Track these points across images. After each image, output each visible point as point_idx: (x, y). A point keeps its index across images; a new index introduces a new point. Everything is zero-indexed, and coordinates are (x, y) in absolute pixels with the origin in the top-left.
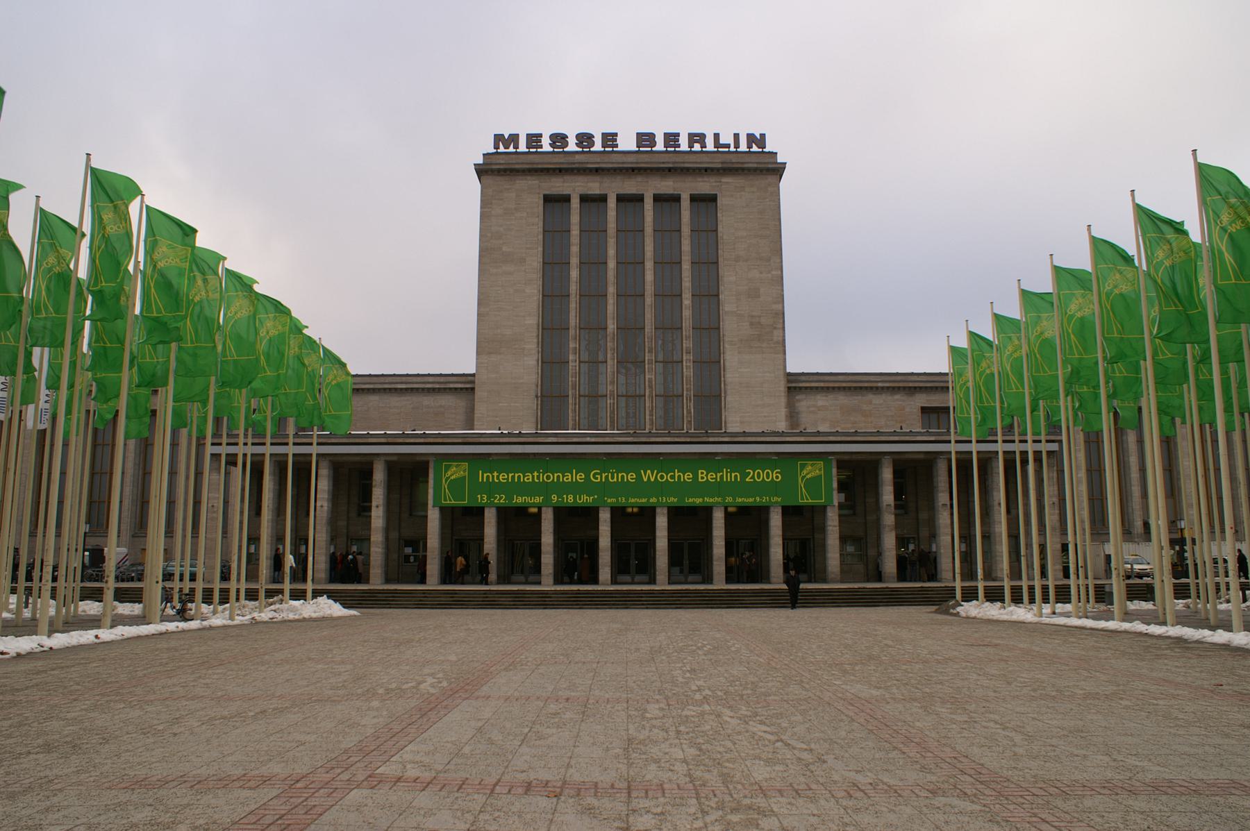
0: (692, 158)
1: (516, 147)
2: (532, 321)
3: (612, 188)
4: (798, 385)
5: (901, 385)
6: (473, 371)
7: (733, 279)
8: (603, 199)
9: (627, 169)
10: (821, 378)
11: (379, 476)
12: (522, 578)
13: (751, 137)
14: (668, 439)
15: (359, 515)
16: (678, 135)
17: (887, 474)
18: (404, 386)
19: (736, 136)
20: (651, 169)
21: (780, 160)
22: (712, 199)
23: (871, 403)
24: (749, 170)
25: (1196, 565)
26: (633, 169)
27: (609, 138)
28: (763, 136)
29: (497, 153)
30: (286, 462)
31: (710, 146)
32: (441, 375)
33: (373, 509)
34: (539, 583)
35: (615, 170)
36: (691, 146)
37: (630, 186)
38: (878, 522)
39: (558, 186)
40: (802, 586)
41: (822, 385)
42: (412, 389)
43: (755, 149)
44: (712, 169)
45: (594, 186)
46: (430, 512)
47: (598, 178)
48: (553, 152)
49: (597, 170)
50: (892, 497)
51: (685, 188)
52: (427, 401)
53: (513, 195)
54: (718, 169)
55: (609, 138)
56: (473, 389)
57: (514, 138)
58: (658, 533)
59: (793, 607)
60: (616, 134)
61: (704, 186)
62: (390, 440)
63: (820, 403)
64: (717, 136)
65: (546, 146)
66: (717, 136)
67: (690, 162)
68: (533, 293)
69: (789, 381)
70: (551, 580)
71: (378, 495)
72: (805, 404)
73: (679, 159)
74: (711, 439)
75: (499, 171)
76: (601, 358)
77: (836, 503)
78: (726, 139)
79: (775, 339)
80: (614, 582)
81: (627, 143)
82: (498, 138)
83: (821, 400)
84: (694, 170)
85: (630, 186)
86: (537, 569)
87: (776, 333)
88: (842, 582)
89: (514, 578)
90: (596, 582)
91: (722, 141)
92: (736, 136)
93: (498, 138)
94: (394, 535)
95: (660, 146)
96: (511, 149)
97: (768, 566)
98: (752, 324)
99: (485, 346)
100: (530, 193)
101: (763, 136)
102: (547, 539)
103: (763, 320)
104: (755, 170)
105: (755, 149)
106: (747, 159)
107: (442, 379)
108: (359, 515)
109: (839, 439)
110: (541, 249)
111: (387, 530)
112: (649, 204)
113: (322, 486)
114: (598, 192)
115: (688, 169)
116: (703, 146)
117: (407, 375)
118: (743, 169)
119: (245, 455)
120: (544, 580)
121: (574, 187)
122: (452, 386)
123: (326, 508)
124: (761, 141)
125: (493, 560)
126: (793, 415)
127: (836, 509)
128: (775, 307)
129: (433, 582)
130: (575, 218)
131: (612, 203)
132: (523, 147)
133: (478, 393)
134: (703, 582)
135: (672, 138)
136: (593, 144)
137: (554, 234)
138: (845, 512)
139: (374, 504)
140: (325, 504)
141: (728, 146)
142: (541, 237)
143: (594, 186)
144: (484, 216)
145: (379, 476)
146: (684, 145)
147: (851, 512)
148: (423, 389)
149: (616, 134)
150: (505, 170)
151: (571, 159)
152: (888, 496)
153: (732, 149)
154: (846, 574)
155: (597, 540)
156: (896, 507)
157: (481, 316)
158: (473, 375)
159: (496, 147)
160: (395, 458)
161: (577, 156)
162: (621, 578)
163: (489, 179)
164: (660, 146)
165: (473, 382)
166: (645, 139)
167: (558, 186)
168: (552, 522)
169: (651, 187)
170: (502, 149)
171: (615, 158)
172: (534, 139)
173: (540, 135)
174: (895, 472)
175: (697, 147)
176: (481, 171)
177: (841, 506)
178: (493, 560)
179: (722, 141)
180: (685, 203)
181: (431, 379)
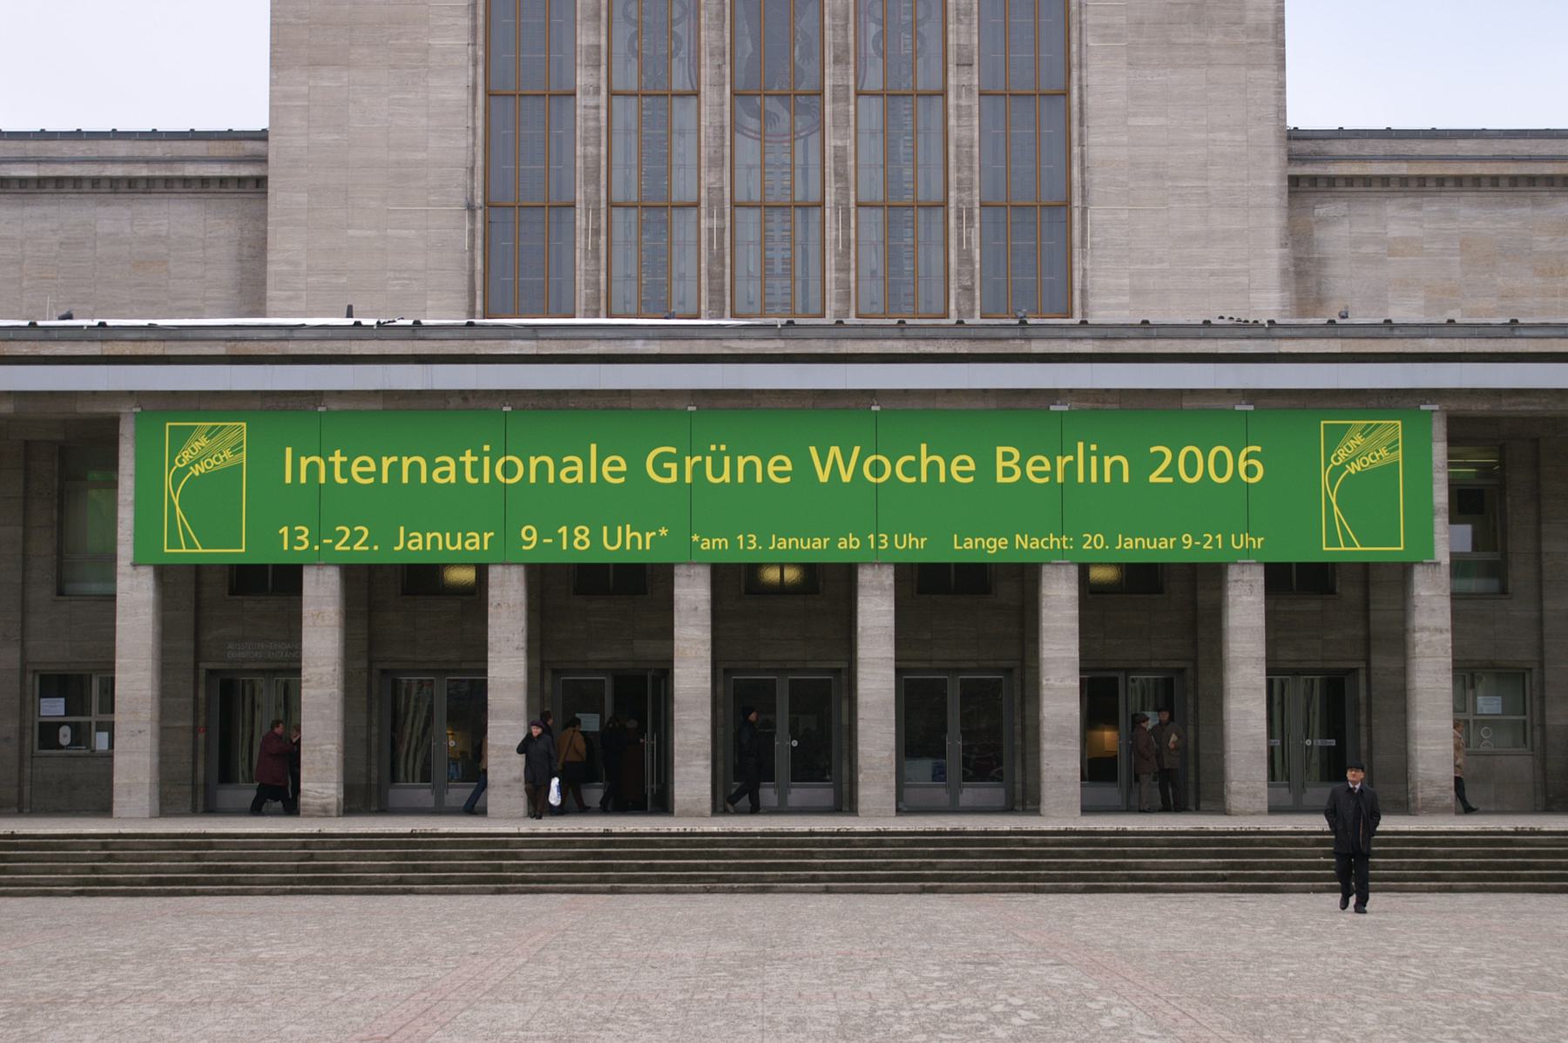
10: (1421, 147)
12: (425, 795)
14: (963, 348)
40: (1387, 824)
41: (1403, 169)
42: (59, 182)
56: (260, 182)
63: (1395, 230)
70: (519, 800)
72: (1345, 230)
74: (1037, 347)
79: (1251, 17)
83: (1398, 220)
89: (398, 795)
102: (507, 669)
109: (1457, 346)
117: (43, 135)
120: (1049, 793)
122: (190, 170)
126: (1304, 271)
127: (1444, 573)
138: (1473, 584)
147: (1493, 584)
148: (96, 182)
158: (262, 136)
165: (262, 160)
168: (521, 612)
177: (1459, 566)
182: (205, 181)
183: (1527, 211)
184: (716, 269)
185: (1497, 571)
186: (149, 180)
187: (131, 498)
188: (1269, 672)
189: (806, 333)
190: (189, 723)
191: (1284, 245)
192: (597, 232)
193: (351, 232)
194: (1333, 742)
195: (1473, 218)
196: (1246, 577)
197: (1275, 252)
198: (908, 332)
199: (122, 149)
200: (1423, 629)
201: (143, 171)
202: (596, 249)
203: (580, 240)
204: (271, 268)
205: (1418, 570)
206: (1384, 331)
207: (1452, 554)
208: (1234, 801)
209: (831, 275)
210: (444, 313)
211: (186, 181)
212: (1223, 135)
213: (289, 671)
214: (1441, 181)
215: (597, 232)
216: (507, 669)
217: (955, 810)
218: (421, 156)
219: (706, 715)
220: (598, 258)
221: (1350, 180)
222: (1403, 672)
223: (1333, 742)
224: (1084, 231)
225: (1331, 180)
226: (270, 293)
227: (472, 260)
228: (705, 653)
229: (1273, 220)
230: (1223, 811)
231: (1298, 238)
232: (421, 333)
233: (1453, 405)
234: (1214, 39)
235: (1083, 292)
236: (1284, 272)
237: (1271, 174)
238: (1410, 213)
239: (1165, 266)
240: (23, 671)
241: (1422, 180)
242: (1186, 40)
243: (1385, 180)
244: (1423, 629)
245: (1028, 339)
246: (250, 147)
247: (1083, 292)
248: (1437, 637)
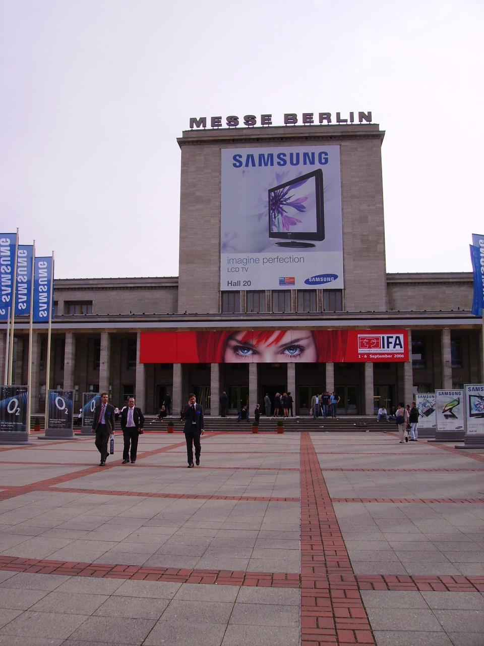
0: (322, 130)
1: (204, 126)
4: (396, 282)
5: (466, 280)
6: (177, 275)
7: (350, 210)
9: (278, 138)
10: (411, 277)
11: (105, 342)
12: (343, 411)
13: (362, 115)
14: (309, 317)
15: (128, 369)
16: (312, 114)
17: (446, 340)
18: (132, 285)
19: (352, 114)
21: (381, 129)
24: (360, 136)
26: (282, 138)
27: (266, 118)
28: (370, 113)
29: (192, 130)
30: (47, 334)
31: (334, 121)
32: (157, 278)
33: (101, 365)
35: (270, 139)
36: (321, 122)
38: (441, 373)
40: (260, 418)
41: (411, 281)
42: (138, 287)
43: (364, 122)
44: (335, 137)
46: (138, 367)
48: (229, 129)
50: (450, 356)
53: (203, 158)
54: (339, 137)
55: (266, 118)
56: (177, 287)
57: (203, 120)
58: (289, 381)
59: (255, 432)
60: (270, 116)
62: (112, 319)
63: (410, 293)
64: (338, 115)
65: (224, 125)
66: (338, 115)
69: (388, 279)
70: (217, 412)
71: (104, 355)
72: (399, 294)
73: (312, 130)
74: (325, 317)
75: (193, 142)
77: (411, 360)
78: (345, 116)
79: (378, 250)
81: (278, 121)
82: (193, 121)
83: (410, 291)
87: (379, 246)
89: (231, 411)
91: (342, 118)
92: (352, 114)
93: (193, 121)
94: (117, 382)
95: (300, 122)
96: (201, 128)
97: (364, 403)
98: (362, 241)
99: (185, 258)
101: (370, 113)
102: (253, 386)
103: (370, 238)
104: (364, 136)
105: (364, 122)
106: (359, 129)
107: (157, 281)
109: (413, 316)
115: (318, 137)
116: (329, 121)
117: (135, 278)
118: (356, 136)
119: (384, 347)
120: (212, 412)
122: (163, 285)
123: (70, 364)
124: (368, 117)
125: (294, 400)
126: (391, 302)
127: (411, 364)
128: (378, 228)
132: (209, 126)
133: (180, 290)
134: (358, 414)
135: (308, 117)
136: (255, 123)
138: (455, 366)
139: (101, 361)
140: (70, 362)
141: (346, 121)
144: (184, 173)
145: (105, 342)
146: (316, 121)
147: (460, 366)
148: (145, 287)
149: (270, 116)
150: (197, 142)
151: (240, 133)
152: (447, 355)
153: (349, 123)
156: (453, 363)
157: (182, 238)
158: (177, 278)
159: (192, 127)
160: (115, 331)
161: (244, 131)
163: (187, 147)
164: (300, 122)
165: (177, 282)
168: (218, 373)
170: (195, 128)
171: (269, 131)
172: (216, 121)
173: (220, 118)
174: (452, 339)
175: (325, 122)
176: (182, 142)
177: (414, 362)
178: (294, 400)
179: (342, 118)
182: (166, 287)
183: (436, 289)
184: (269, 303)
185: (459, 363)
186: (155, 287)
187: (139, 350)
188: (374, 385)
189: (276, 314)
190: (153, 396)
191: (386, 297)
192: (244, 296)
193: (195, 297)
194: (390, 400)
195: (425, 290)
196: (369, 365)
197: (384, 298)
198: (298, 314)
199: (150, 281)
200: (407, 376)
201: (154, 285)
202: (244, 300)
203: (241, 298)
204: (179, 304)
205: (405, 363)
206: (398, 313)
207: (413, 360)
208: (367, 413)
209: (292, 304)
210: (214, 311)
211: (162, 287)
212: (373, 274)
213: (171, 385)
214: (419, 283)
215: (244, 296)
216: (253, 386)
217: (347, 415)
218: (209, 281)
219: (256, 394)
220: (244, 301)
221: (400, 283)
222: (403, 386)
223: (390, 400)
224: (344, 294)
225: (396, 283)
226: (179, 309)
227: (219, 302)
228: (256, 381)
229: (383, 291)
230: (365, 414)
231: (389, 295)
232: (197, 315)
233: (412, 328)
234: (370, 255)
235: (345, 307)
236: (386, 302)
237: (383, 282)
238: (413, 290)
239: (361, 301)
240: (120, 385)
241: (415, 283)
242: (365, 255)
243: (407, 283)
244: (407, 376)
245: (323, 315)
246: (176, 280)
247: (345, 307)
248: (409, 378)
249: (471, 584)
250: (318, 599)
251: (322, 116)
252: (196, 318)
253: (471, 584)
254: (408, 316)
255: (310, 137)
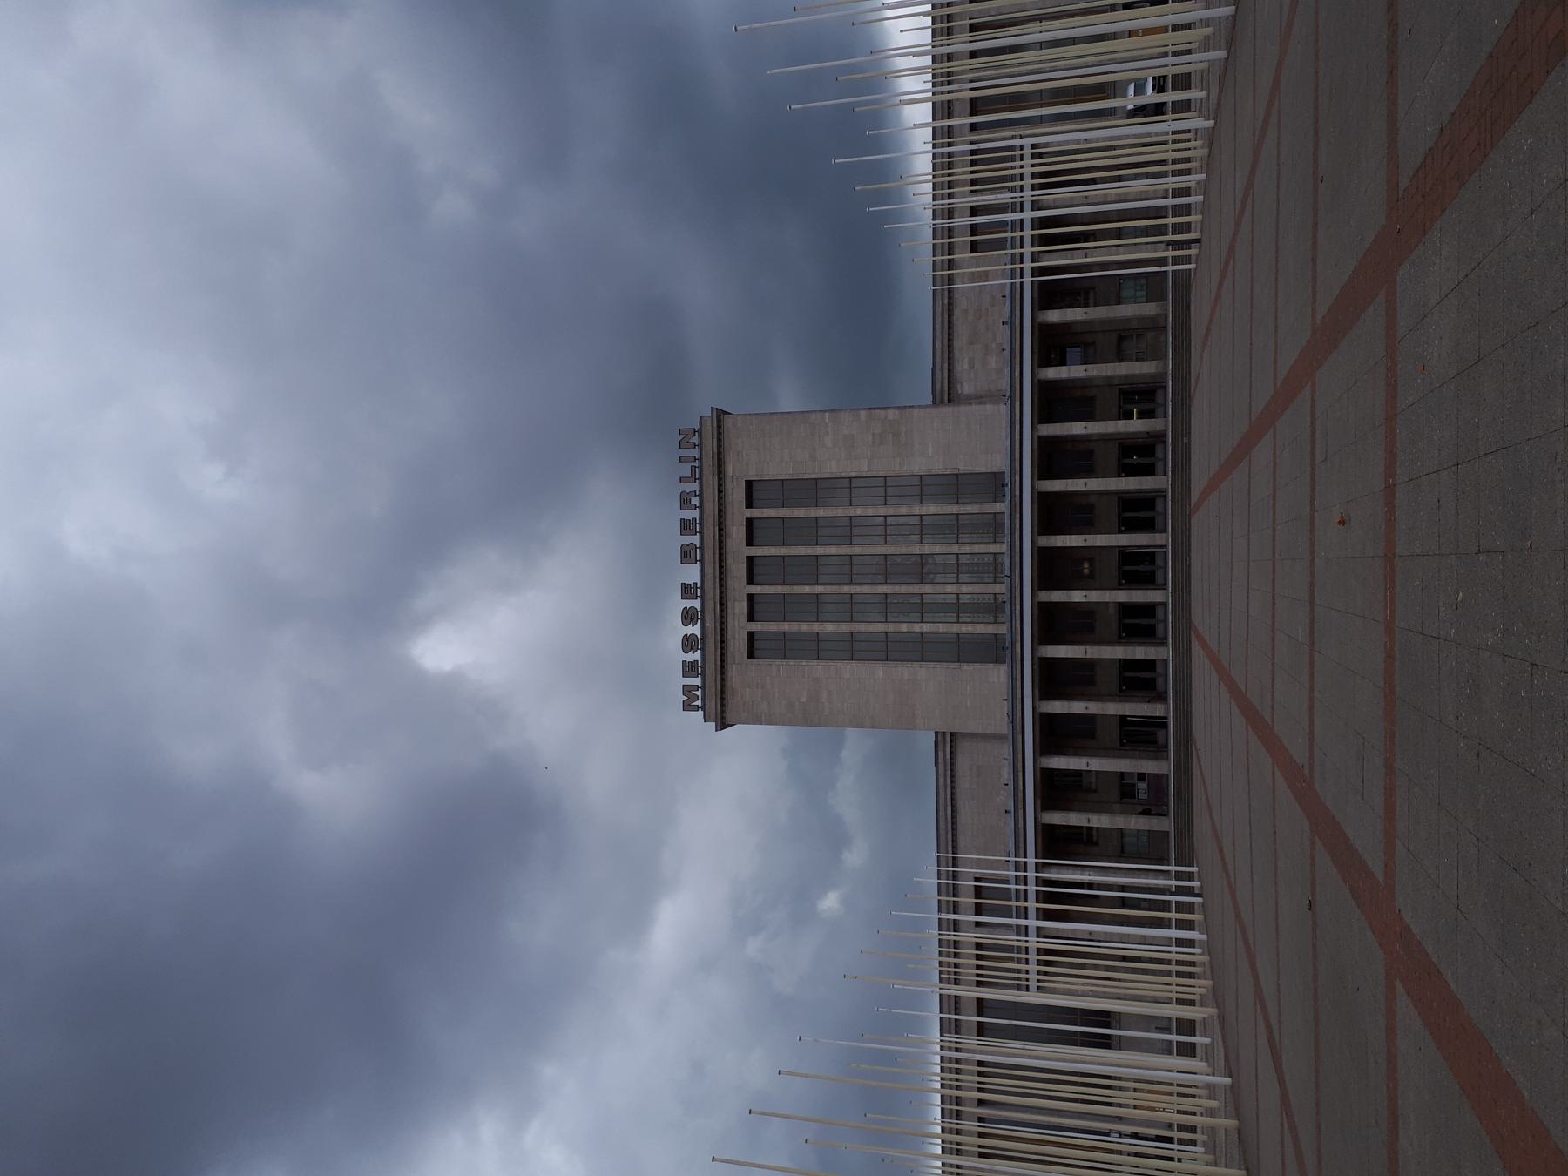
2: (879, 671)
3: (739, 588)
8: (751, 598)
9: (721, 573)
11: (1056, 818)
15: (1097, 844)
17: (1054, 316)
20: (721, 548)
22: (749, 485)
23: (966, 311)
24: (719, 447)
25: (1194, 1096)
27: (687, 591)
34: (1166, 661)
35: (721, 586)
37: (738, 569)
39: (738, 644)
44: (720, 485)
45: (738, 608)
47: (729, 604)
48: (703, 649)
49: (721, 604)
51: (738, 514)
52: (964, 784)
56: (952, 734)
57: (687, 690)
61: (736, 494)
63: (966, 366)
66: (682, 480)
67: (711, 507)
68: (849, 669)
69: (942, 402)
70: (1161, 649)
71: (1074, 819)
75: (722, 705)
76: (917, 600)
80: (1164, 586)
81: (692, 574)
82: (687, 706)
83: (962, 366)
84: (720, 504)
85: (738, 569)
86: (1150, 665)
88: (1166, 357)
90: (1165, 604)
93: (687, 706)
96: (699, 693)
100: (743, 673)
108: (1097, 844)
110: (804, 663)
111: (1110, 812)
112: (755, 551)
113: (1067, 873)
114: (745, 604)
115: (720, 511)
118: (719, 453)
121: (739, 627)
129: (1167, 824)
130: (773, 627)
131: (755, 589)
135: (686, 526)
137: (788, 648)
142: (792, 662)
143: (738, 608)
145: (1056, 818)
154: (1158, 355)
155: (1120, 604)
162: (1159, 579)
166: (687, 555)
167: (738, 644)
169: (738, 550)
170: (699, 703)
172: (688, 669)
175: (695, 501)
176: (723, 724)
180: (754, 513)
181: (941, 779)
222: (1120, 377)
249: (1391, 6)
250: (964, 747)
251: (685, 503)
252: (1015, 698)
253: (1391, 6)
254: (1017, 374)
255: (720, 523)
